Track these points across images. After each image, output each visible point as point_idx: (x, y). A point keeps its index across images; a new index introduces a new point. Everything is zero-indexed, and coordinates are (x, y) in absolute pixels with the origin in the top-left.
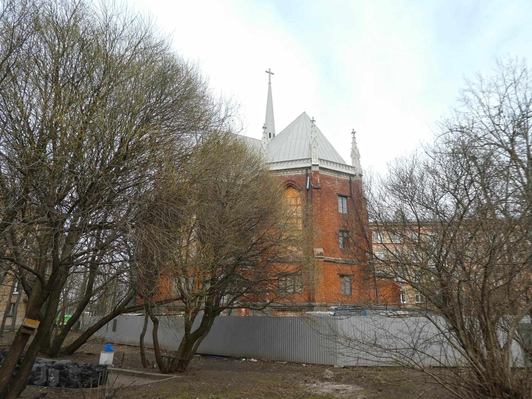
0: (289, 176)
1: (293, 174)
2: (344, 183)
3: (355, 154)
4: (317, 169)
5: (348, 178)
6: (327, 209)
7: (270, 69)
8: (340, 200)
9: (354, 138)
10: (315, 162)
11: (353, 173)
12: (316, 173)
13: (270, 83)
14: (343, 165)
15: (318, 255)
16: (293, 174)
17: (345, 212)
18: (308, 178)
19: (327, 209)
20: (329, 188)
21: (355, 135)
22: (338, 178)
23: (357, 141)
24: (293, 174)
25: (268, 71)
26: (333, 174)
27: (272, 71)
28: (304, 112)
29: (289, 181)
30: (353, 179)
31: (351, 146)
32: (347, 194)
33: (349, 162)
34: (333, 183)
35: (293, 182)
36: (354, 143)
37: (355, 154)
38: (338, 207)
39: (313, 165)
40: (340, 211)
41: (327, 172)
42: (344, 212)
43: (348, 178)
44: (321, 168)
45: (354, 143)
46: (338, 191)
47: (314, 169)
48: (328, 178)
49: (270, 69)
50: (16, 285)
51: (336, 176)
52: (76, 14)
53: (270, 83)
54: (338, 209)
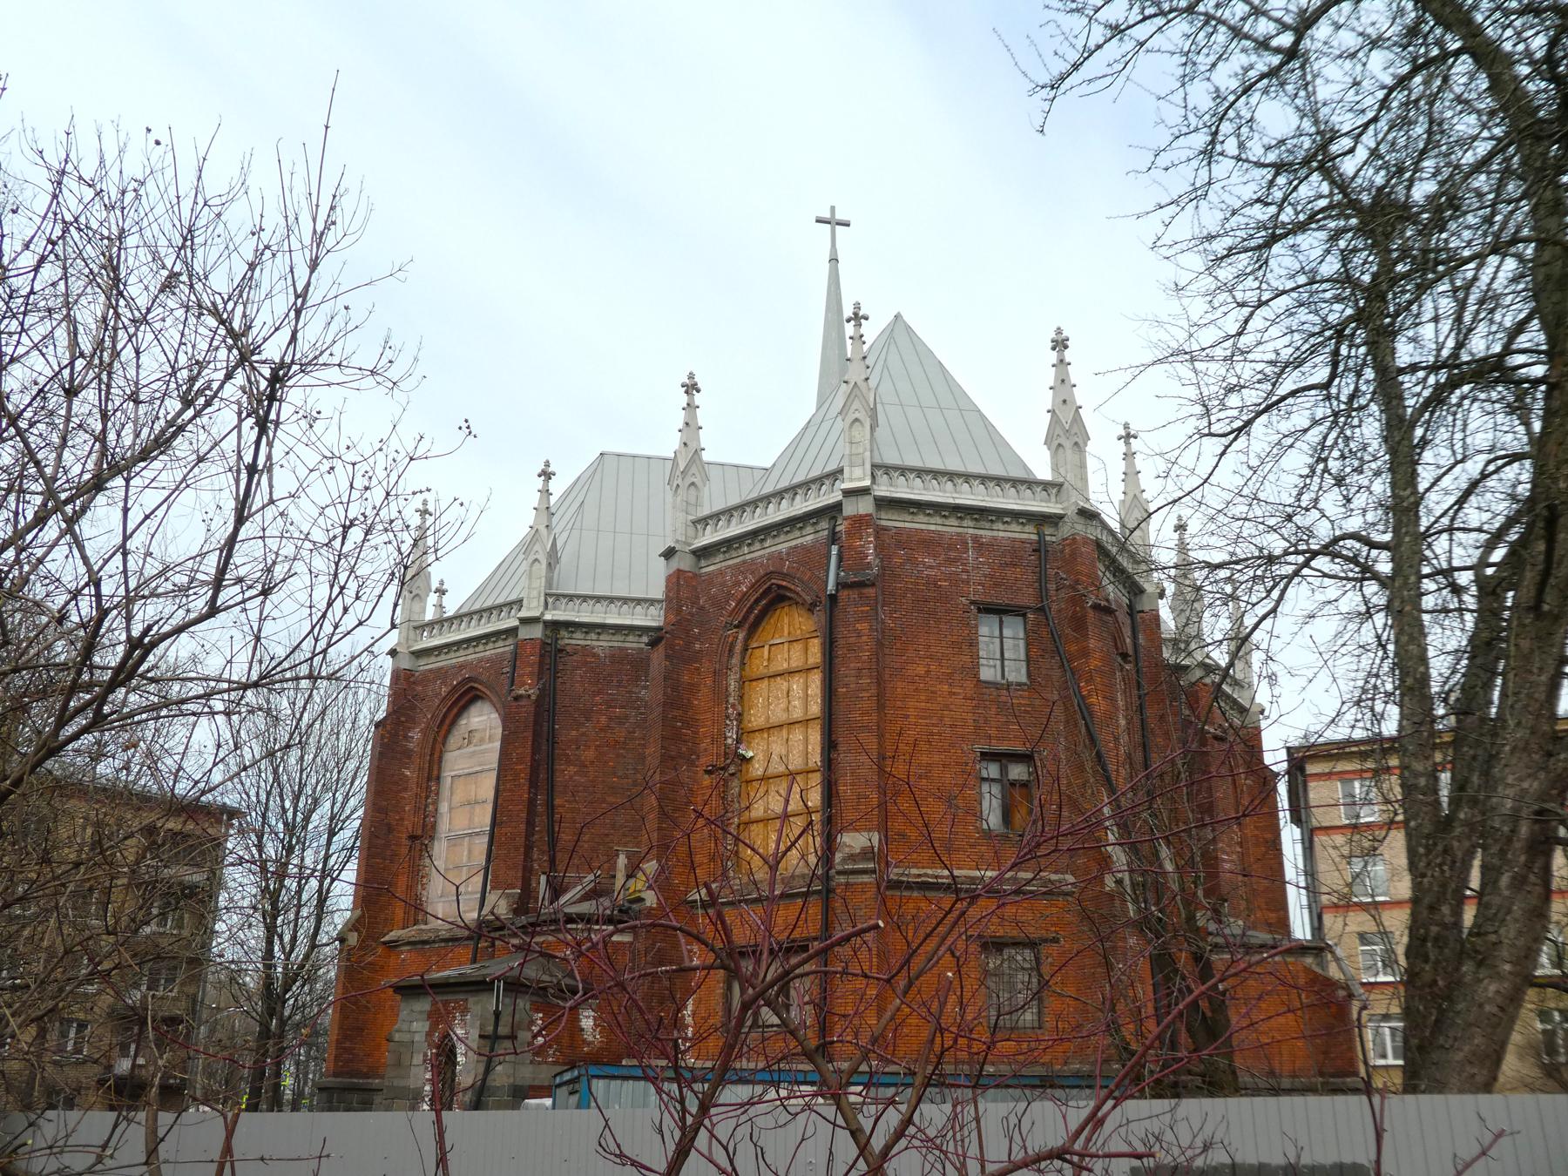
0: (771, 557)
1: (783, 547)
2: (1013, 552)
3: (1067, 433)
4: (864, 506)
5: (1028, 533)
6: (921, 670)
7: (833, 209)
8: (987, 629)
9: (1062, 363)
10: (857, 478)
11: (1052, 508)
12: (860, 522)
13: (834, 260)
14: (1023, 482)
15: (852, 858)
16: (781, 545)
17: (1017, 673)
18: (835, 550)
19: (921, 670)
20: (933, 583)
21: (1068, 355)
22: (976, 539)
23: (1074, 374)
24: (781, 545)
25: (827, 215)
26: (953, 521)
27: (839, 216)
28: (898, 317)
29: (769, 575)
30: (1051, 536)
31: (1047, 400)
32: (1026, 598)
33: (1042, 470)
34: (951, 561)
35: (784, 576)
36: (1063, 382)
37: (1067, 433)
38: (976, 657)
39: (848, 493)
40: (987, 674)
41: (921, 518)
42: (1012, 677)
43: (1028, 533)
44: (885, 503)
45: (1063, 382)
46: (976, 592)
47: (849, 509)
48: (929, 543)
49: (833, 209)
50: (1469, 915)
51: (969, 529)
52: (865, 365)
53: (834, 260)
54: (976, 666)
